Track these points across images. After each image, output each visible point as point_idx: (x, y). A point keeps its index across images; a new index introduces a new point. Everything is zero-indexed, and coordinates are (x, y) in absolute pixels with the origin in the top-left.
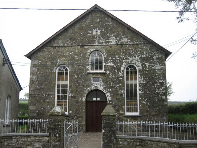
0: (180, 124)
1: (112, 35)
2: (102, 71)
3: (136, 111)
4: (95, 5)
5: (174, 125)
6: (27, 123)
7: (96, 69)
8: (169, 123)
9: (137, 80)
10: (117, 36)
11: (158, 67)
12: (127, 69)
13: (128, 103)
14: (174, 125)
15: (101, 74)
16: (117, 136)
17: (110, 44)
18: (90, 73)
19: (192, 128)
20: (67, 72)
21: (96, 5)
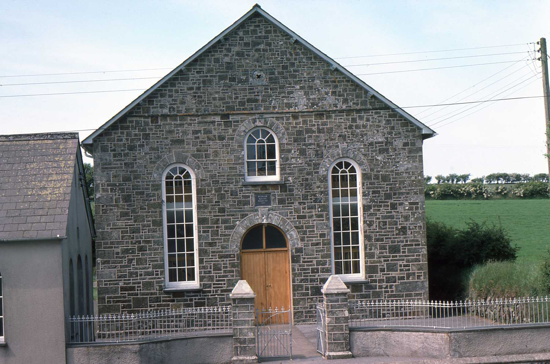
0: (542, 299)
1: (298, 87)
2: (276, 178)
3: (357, 270)
4: (254, 7)
5: (442, 305)
6: (464, 308)
7: (262, 172)
8: (99, 316)
9: (356, 196)
10: (309, 90)
11: (404, 165)
12: (335, 170)
13: (365, 215)
14: (442, 305)
15: (274, 185)
16: (168, 118)
17: (292, 110)
18: (246, 185)
19: (450, 309)
20: (190, 182)
21: (257, 6)
